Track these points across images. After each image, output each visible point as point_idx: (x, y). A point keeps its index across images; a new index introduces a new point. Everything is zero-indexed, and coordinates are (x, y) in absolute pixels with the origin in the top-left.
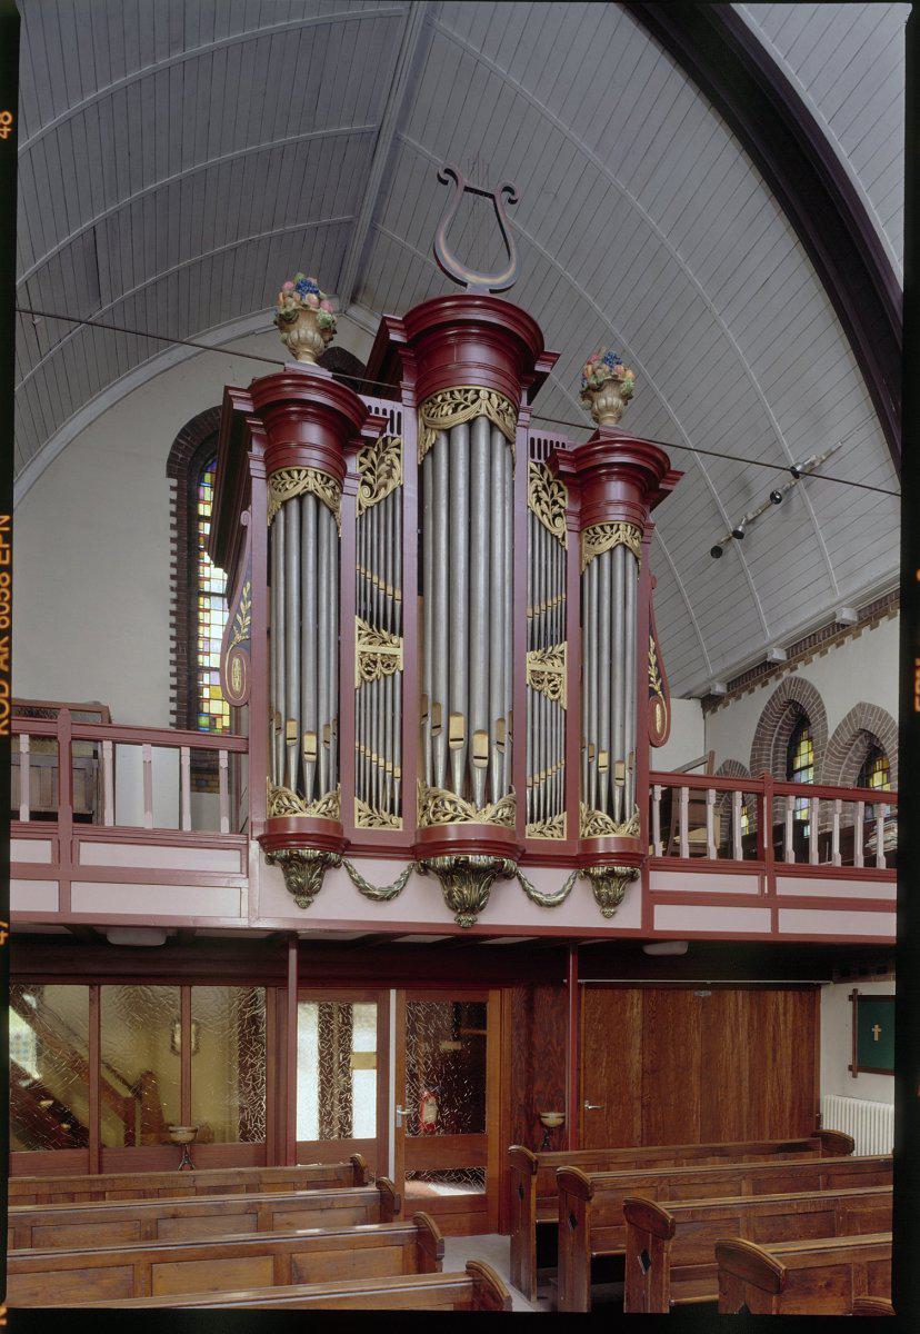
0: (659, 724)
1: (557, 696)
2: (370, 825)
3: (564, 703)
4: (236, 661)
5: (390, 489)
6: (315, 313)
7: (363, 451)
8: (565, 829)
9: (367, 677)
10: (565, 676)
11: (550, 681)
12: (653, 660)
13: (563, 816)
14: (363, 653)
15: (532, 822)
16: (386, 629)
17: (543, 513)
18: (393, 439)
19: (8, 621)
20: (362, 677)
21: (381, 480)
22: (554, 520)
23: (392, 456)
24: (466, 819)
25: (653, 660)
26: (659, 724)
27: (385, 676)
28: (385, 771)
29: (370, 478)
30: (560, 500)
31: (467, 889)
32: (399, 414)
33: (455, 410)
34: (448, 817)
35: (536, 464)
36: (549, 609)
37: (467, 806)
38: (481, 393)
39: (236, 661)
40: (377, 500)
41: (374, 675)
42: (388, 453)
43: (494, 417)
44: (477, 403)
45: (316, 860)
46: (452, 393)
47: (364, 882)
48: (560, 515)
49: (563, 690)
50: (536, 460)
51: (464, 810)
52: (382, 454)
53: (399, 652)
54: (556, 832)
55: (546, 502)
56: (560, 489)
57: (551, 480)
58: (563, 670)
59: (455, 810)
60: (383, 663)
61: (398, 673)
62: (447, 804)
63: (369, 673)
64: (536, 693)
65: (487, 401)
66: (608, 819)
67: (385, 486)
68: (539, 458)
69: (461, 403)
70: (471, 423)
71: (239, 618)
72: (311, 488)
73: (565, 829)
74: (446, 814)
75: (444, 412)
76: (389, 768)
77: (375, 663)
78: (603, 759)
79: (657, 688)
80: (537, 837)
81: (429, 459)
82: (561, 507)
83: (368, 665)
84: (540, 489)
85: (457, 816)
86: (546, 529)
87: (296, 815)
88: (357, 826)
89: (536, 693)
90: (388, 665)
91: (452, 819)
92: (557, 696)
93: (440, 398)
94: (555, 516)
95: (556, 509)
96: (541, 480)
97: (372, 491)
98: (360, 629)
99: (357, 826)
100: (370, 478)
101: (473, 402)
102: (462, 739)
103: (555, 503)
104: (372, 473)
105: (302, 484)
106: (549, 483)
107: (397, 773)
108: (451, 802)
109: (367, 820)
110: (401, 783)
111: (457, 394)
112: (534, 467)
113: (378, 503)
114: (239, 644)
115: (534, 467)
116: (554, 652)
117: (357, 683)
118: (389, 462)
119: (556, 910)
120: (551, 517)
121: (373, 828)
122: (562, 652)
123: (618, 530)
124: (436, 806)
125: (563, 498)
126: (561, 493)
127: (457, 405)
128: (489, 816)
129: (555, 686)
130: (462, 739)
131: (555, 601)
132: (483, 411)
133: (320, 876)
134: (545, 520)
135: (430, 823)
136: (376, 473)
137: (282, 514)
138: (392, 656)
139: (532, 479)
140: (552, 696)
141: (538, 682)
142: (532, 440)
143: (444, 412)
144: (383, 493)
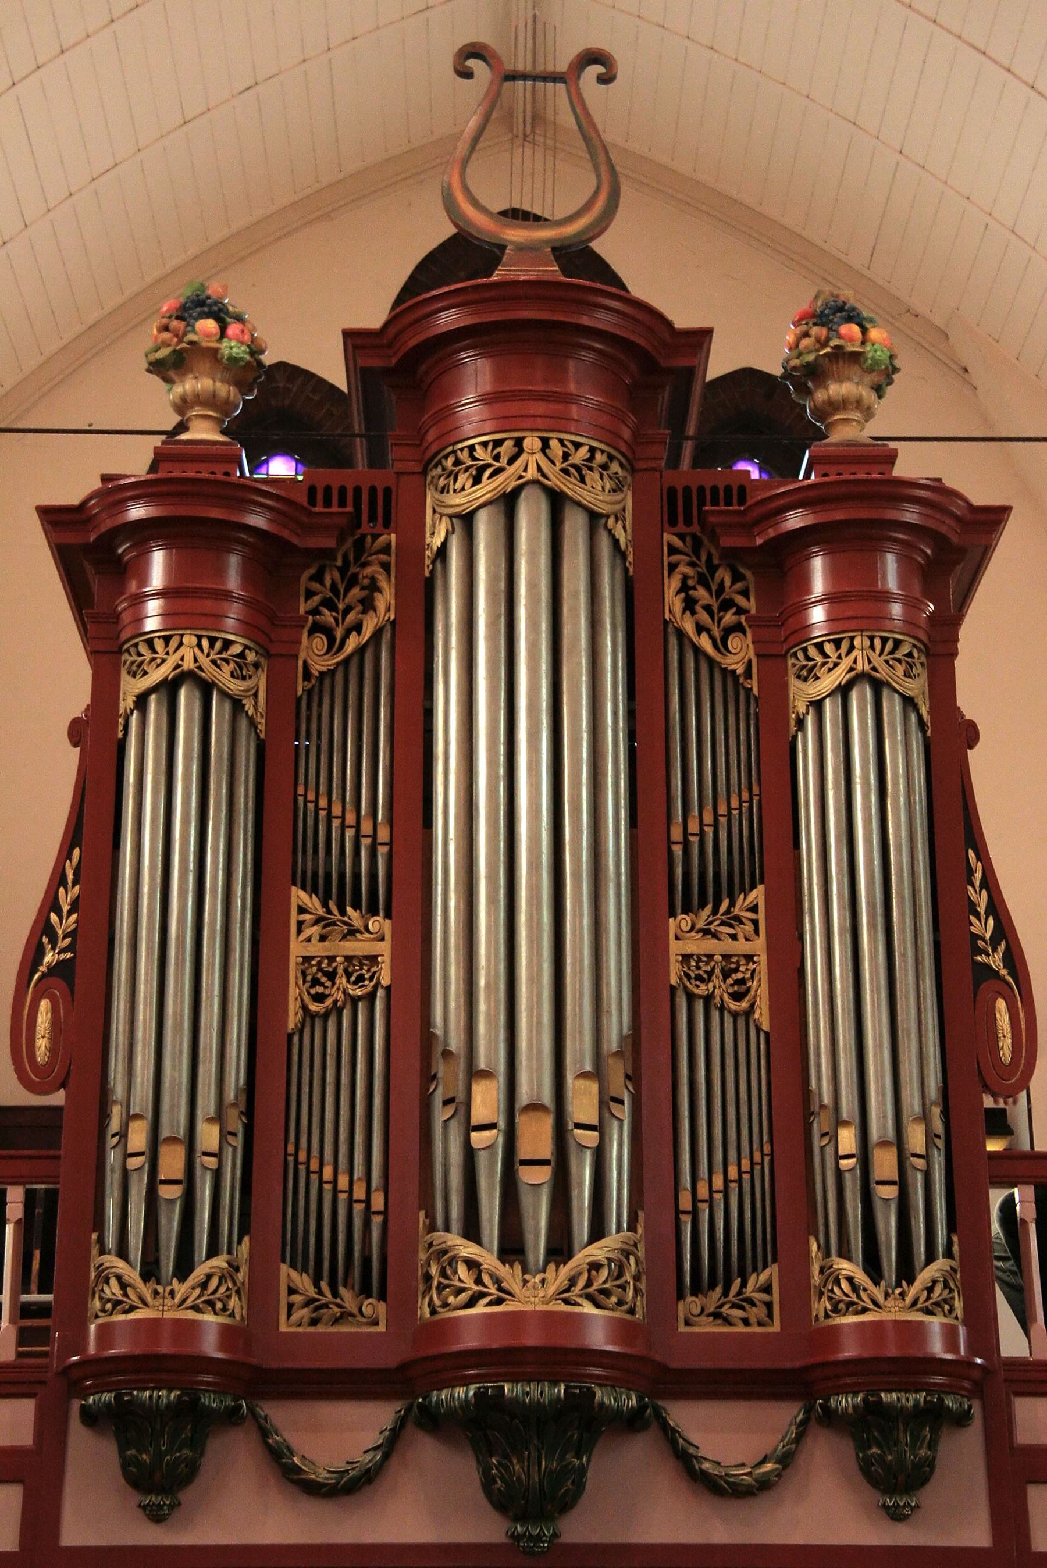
0: (1006, 1044)
1: (744, 1004)
2: (314, 1322)
3: (762, 1016)
4: (44, 1005)
5: (368, 630)
6: (216, 351)
7: (312, 571)
8: (301, 1330)
9: (314, 1007)
10: (763, 959)
11: (726, 974)
12: (982, 901)
13: (771, 1273)
14: (307, 959)
15: (696, 1290)
16: (356, 906)
17: (700, 629)
18: (375, 537)
19: (738, 650)
20: (304, 1007)
21: (351, 617)
22: (724, 640)
23: (373, 569)
24: (499, 1301)
25: (982, 901)
26: (1006, 1044)
27: (354, 1001)
28: (351, 1201)
29: (328, 617)
30: (740, 600)
31: (520, 1461)
32: (388, 491)
33: (477, 480)
34: (464, 1297)
35: (682, 537)
36: (723, 820)
37: (503, 1271)
38: (526, 444)
39: (44, 1005)
40: (341, 657)
41: (329, 1002)
42: (364, 565)
43: (556, 481)
44: (519, 463)
45: (177, 1410)
46: (472, 448)
47: (292, 1453)
48: (738, 628)
49: (761, 990)
50: (681, 528)
51: (498, 1281)
52: (353, 570)
53: (384, 949)
54: (756, 1313)
55: (708, 608)
56: (737, 577)
57: (716, 561)
58: (759, 946)
59: (479, 1281)
60: (348, 975)
61: (380, 993)
62: (462, 1270)
63: (319, 998)
64: (699, 1007)
65: (539, 457)
66: (861, 1277)
67: (358, 628)
68: (688, 522)
69: (489, 465)
70: (508, 502)
71: (54, 917)
72: (188, 664)
73: (301, 1330)
74: (462, 1290)
75: (458, 485)
76: (359, 1193)
77: (332, 976)
78: (847, 1139)
79: (996, 961)
80: (707, 1327)
81: (439, 565)
82: (740, 611)
83: (315, 982)
84: (690, 583)
85: (482, 1295)
86: (711, 662)
87: (132, 1316)
88: (283, 1328)
89: (699, 1007)
90: (361, 979)
91: (471, 1303)
92: (744, 1004)
93: (451, 460)
94: (728, 631)
95: (729, 618)
96: (692, 564)
97: (331, 640)
98: (302, 910)
99: (283, 1328)
100: (328, 617)
101: (511, 461)
102: (492, 1126)
103: (727, 605)
104: (333, 608)
105: (172, 660)
106: (712, 569)
107: (378, 1202)
108: (472, 1264)
109: (305, 1311)
110: (385, 1224)
111: (479, 452)
112: (677, 542)
113: (346, 661)
114: (55, 970)
115: (677, 542)
116: (736, 911)
117: (293, 1020)
118: (366, 582)
119: (762, 1502)
120: (717, 633)
121: (320, 1329)
122: (754, 909)
123: (852, 648)
124: (443, 1274)
125: (745, 593)
126: (739, 586)
127: (481, 470)
128: (552, 1289)
129: (741, 982)
130: (492, 1126)
131: (735, 803)
132: (531, 473)
133: (933, 1445)
134: (705, 642)
135: (433, 1312)
136: (341, 606)
137: (134, 718)
138: (366, 957)
139: (673, 567)
140: (734, 1005)
141: (699, 978)
142: (672, 492)
143: (458, 485)
144: (352, 643)
